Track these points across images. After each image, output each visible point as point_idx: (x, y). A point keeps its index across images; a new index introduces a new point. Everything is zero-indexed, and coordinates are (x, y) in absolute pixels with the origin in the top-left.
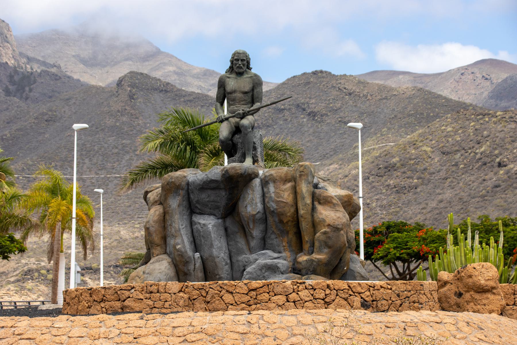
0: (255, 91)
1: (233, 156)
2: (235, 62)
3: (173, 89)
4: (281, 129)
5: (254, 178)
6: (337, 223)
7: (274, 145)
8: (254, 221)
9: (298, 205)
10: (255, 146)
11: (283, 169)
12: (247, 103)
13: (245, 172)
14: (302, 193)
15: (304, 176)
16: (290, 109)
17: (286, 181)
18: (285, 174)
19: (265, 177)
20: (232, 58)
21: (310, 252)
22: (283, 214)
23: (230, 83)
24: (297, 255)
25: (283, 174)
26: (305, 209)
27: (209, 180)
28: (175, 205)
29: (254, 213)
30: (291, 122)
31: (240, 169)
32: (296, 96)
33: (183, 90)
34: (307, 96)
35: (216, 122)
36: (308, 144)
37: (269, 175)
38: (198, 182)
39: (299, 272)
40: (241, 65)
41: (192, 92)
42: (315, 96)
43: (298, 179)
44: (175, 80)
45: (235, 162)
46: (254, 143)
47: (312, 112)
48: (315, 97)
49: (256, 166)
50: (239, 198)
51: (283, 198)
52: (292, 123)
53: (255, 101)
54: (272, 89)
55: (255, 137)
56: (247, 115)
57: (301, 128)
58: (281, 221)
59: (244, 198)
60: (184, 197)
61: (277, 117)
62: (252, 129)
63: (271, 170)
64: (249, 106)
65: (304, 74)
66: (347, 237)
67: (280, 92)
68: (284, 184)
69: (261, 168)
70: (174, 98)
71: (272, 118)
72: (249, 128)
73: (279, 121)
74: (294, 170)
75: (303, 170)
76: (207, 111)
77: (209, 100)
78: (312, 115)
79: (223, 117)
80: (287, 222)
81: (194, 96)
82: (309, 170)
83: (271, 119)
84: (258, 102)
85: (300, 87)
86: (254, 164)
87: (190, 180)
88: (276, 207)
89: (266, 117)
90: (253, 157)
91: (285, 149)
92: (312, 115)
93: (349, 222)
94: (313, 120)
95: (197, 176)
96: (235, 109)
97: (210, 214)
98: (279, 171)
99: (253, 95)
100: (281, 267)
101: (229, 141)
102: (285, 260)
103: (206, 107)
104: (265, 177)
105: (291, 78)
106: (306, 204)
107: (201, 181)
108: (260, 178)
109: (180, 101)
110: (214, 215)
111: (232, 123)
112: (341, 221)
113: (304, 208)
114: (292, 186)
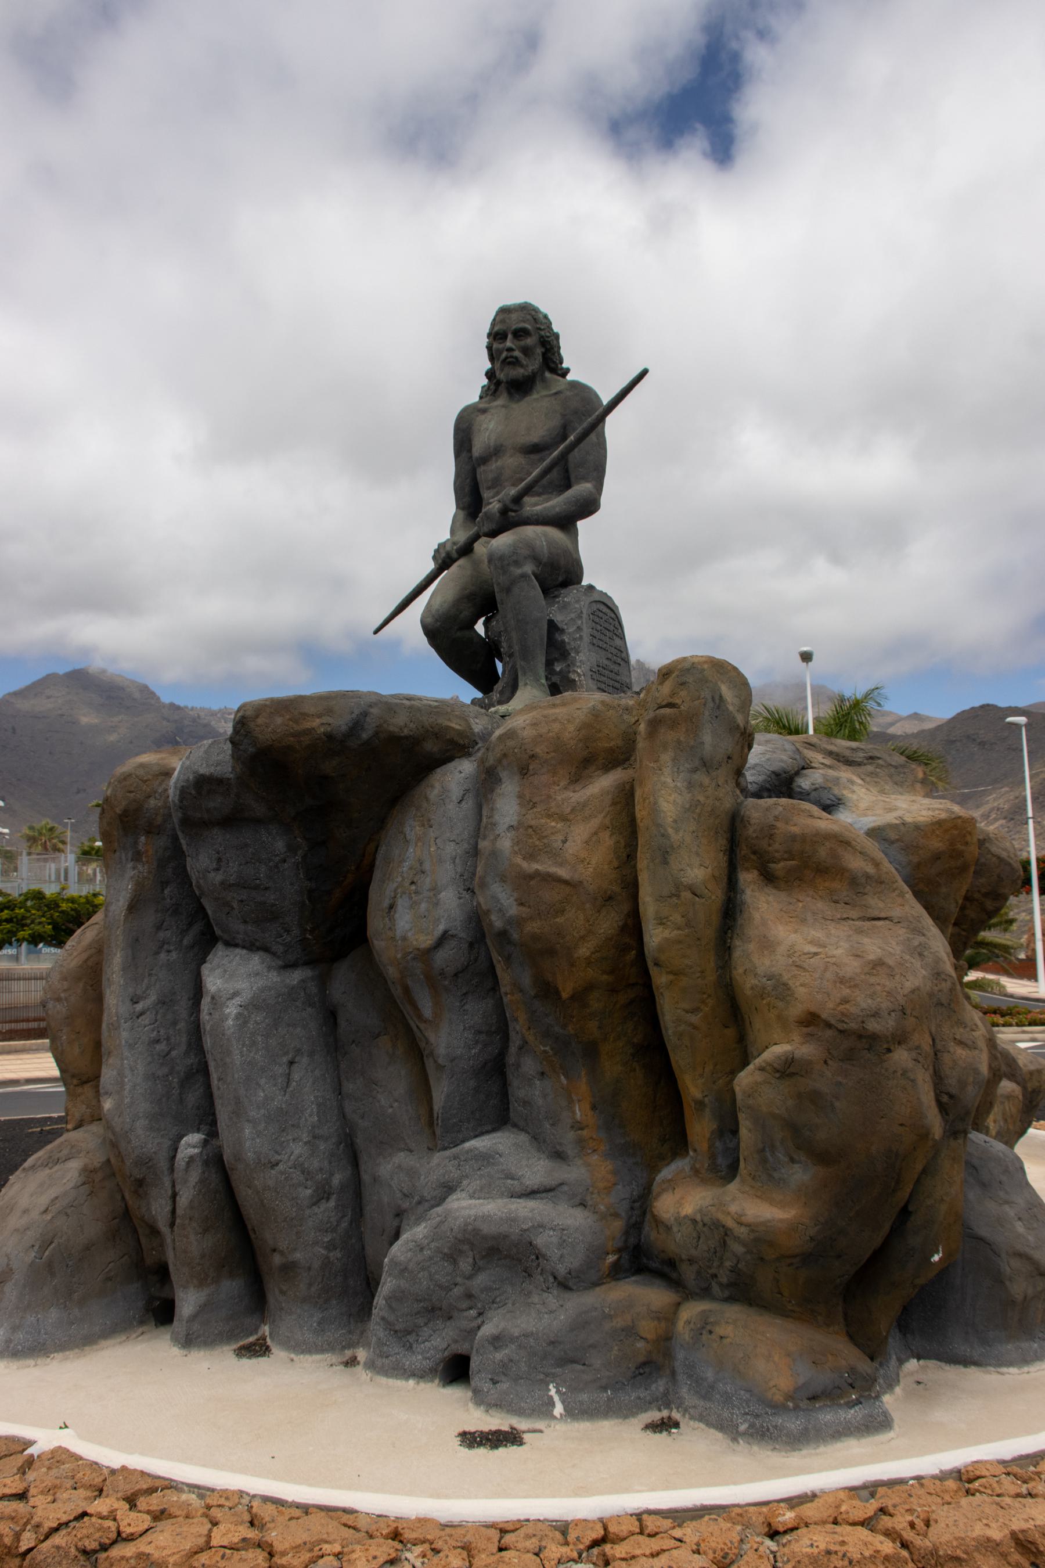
6: (863, 1001)
8: (432, 981)
15: (674, 724)
18: (585, 726)
21: (722, 1162)
22: (551, 952)
24: (653, 1169)
25: (571, 728)
26: (676, 918)
29: (425, 941)
31: (329, 711)
39: (666, 1269)
40: (517, 353)
47: (982, 742)
50: (372, 866)
51: (555, 855)
53: (573, 479)
58: (547, 991)
65: (973, 708)
66: (938, 1079)
75: (673, 694)
78: (982, 744)
80: (580, 997)
84: (584, 479)
88: (514, 910)
92: (982, 744)
93: (946, 986)
97: (252, 946)
98: (557, 711)
100: (554, 1253)
102: (583, 1204)
110: (266, 949)
112: (889, 984)
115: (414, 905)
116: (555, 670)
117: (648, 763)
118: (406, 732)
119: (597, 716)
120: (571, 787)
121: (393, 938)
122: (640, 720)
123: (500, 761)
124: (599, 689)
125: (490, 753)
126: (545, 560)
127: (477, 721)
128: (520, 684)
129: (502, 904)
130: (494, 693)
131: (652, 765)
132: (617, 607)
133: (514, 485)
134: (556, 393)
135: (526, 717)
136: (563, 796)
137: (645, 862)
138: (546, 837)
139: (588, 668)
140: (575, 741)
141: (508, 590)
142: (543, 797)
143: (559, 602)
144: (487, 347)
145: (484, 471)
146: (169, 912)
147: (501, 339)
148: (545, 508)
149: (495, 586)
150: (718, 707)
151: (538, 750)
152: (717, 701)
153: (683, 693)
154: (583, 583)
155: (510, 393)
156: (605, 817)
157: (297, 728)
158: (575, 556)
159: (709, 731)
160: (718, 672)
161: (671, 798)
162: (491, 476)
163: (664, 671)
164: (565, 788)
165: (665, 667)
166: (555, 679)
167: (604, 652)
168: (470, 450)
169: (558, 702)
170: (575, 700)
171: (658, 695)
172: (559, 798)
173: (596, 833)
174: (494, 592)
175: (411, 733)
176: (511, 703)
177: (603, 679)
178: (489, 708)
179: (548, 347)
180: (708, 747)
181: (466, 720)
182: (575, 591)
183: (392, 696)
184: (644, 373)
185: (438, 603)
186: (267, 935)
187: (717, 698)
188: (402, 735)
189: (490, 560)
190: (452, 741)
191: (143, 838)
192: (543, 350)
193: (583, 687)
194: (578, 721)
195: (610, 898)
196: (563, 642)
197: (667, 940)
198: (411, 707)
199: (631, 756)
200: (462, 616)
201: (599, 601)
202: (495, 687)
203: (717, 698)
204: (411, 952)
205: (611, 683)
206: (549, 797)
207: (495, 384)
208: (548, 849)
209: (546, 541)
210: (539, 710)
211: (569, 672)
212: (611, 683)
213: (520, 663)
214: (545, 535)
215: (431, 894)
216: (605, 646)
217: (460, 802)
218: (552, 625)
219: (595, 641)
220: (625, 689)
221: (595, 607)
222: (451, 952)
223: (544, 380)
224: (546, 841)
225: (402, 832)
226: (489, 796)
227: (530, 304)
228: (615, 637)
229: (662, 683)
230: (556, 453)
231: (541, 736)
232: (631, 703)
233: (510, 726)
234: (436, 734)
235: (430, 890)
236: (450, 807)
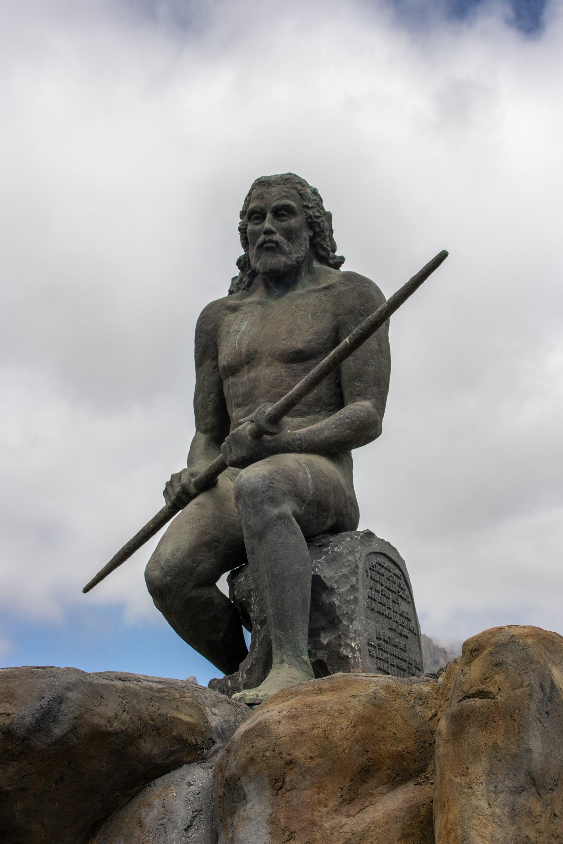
25: (344, 723)
40: (277, 237)
75: (485, 679)
84: (362, 395)
98: (324, 698)
116: (321, 643)
118: (116, 725)
119: (378, 707)
122: (439, 715)
123: (244, 769)
124: (379, 669)
125: (231, 758)
126: (310, 498)
127: (216, 711)
128: (274, 661)
130: (240, 672)
131: (458, 780)
132: (403, 561)
133: (272, 401)
134: (327, 288)
135: (281, 706)
136: (333, 822)
139: (365, 641)
140: (349, 742)
141: (261, 535)
142: (304, 824)
143: (328, 552)
144: (240, 229)
145: (232, 383)
147: (257, 218)
148: (310, 431)
149: (244, 530)
150: (550, 699)
151: (298, 753)
152: (548, 691)
153: (499, 678)
154: (358, 530)
155: (268, 288)
158: (348, 494)
159: (537, 733)
160: (547, 648)
162: (241, 390)
163: (472, 646)
165: (472, 640)
166: (322, 655)
167: (386, 620)
168: (215, 358)
169: (326, 686)
170: (349, 683)
172: (327, 825)
174: (242, 538)
175: (123, 728)
176: (261, 687)
177: (385, 656)
178: (233, 693)
179: (317, 230)
180: (537, 756)
181: (201, 710)
182: (348, 539)
183: (100, 675)
184: (442, 257)
185: (169, 551)
187: (547, 684)
188: (111, 729)
189: (238, 497)
190: (179, 739)
192: (311, 234)
193: (357, 666)
194: (353, 713)
196: (332, 605)
198: (124, 690)
199: (427, 765)
200: (200, 568)
201: (380, 553)
202: (242, 665)
203: (547, 684)
205: (396, 662)
206: (313, 823)
207: (249, 275)
209: (311, 473)
210: (301, 696)
211: (340, 646)
212: (396, 662)
213: (275, 632)
214: (310, 465)
216: (387, 612)
217: (187, 829)
218: (318, 583)
219: (374, 606)
220: (415, 670)
221: (374, 560)
223: (311, 271)
226: (229, 821)
227: (295, 176)
228: (400, 600)
229: (469, 662)
230: (326, 360)
231: (303, 734)
232: (426, 689)
233: (260, 719)
234: (158, 729)
236: (173, 836)
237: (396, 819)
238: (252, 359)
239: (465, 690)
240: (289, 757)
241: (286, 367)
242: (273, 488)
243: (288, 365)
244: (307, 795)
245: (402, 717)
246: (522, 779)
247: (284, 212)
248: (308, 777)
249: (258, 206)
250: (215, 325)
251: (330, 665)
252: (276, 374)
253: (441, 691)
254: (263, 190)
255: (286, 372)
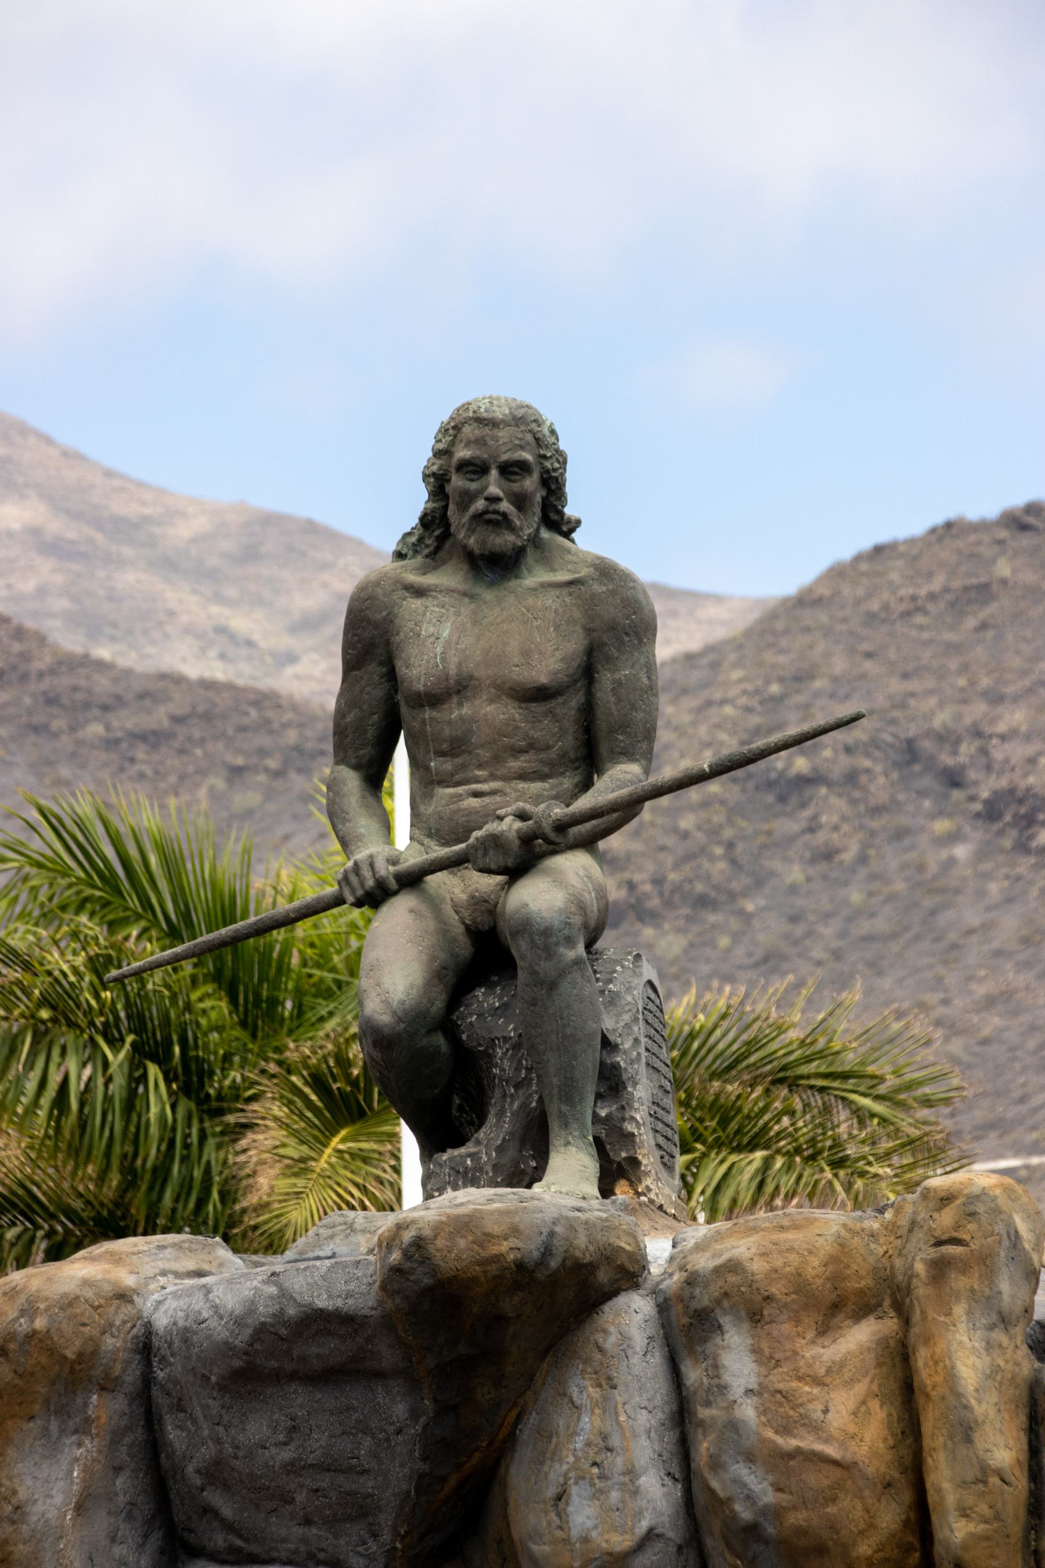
0: (606, 679)
1: (460, 1141)
2: (457, 482)
3: (26, 657)
4: (794, 919)
5: (614, 1293)
7: (752, 1046)
9: (931, 1480)
10: (616, 1067)
11: (810, 1221)
12: (552, 764)
13: (547, 1251)
14: (959, 1395)
15: (964, 1266)
16: (851, 778)
17: (836, 1307)
19: (692, 1280)
20: (438, 454)
23: (427, 629)
25: (815, 1261)
26: (984, 1509)
27: (292, 1311)
28: (58, 1499)
29: (621, 1542)
30: (863, 872)
31: (515, 1231)
32: (896, 686)
33: (101, 665)
34: (972, 683)
35: (338, 901)
36: (993, 1022)
37: (717, 1271)
38: (219, 1331)
40: (505, 506)
41: (163, 676)
42: (1027, 682)
43: (921, 1290)
44: (42, 592)
45: (474, 1182)
46: (607, 1044)
48: (1030, 691)
49: (626, 1208)
50: (511, 1439)
51: (816, 1428)
52: (873, 877)
53: (603, 749)
54: (726, 643)
55: (613, 1000)
56: (555, 850)
57: (933, 913)
59: (545, 1434)
60: (116, 1438)
61: (762, 839)
62: (589, 946)
63: (730, 1233)
64: (567, 782)
67: (782, 659)
68: (824, 1331)
69: (662, 1220)
70: (38, 719)
71: (730, 846)
72: (570, 942)
73: (777, 865)
74: (891, 1228)
75: (957, 1227)
76: (271, 807)
77: (285, 726)
79: (384, 870)
81: (179, 705)
82: (1000, 1228)
83: (719, 851)
84: (627, 754)
85: (919, 619)
86: (606, 1191)
87: (161, 1321)
88: (769, 1497)
89: (685, 835)
90: (599, 1144)
91: (827, 1076)
94: (1023, 847)
95: (207, 1290)
96: (471, 812)
98: (790, 1235)
99: (588, 711)
101: (430, 1032)
103: (262, 778)
104: (692, 1280)
105: (858, 558)
106: (984, 1472)
107: (239, 1322)
108: (654, 1292)
109: (80, 743)
111: (448, 909)
113: (970, 1500)
114: (883, 1343)
115: (598, 1494)
117: (935, 1315)
120: (819, 1341)
121: (566, 1541)
123: (718, 1302)
129: (750, 1490)
137: (941, 1439)
138: (802, 1405)
140: (821, 1280)
142: (788, 1354)
146: (123, 1515)
152: (1013, 1238)
153: (972, 1227)
156: (872, 1382)
157: (483, 1254)
159: (1006, 1277)
161: (970, 1362)
164: (813, 1342)
171: (934, 1226)
172: (808, 1355)
173: (864, 1402)
180: (1006, 1297)
186: (342, 1542)
187: (1012, 1232)
191: (95, 1397)
194: (823, 1252)
195: (889, 1485)
197: (972, 1535)
200: (434, 1009)
203: (1012, 1232)
204: (596, 1559)
206: (795, 1353)
208: (806, 1421)
211: (624, 1119)
215: (627, 1479)
222: (654, 1558)
224: (801, 1410)
225: (565, 1394)
231: (776, 1271)
235: (624, 1474)
237: (869, 1349)
238: (465, 687)
239: (936, 1235)
240: (766, 1293)
241: (520, 708)
242: (570, 924)
243: (523, 705)
244: (786, 1328)
245: (862, 1255)
246: (994, 1317)
247: (516, 470)
248: (785, 1312)
249: (478, 458)
250: (389, 614)
251: (610, 1144)
252: (507, 717)
253: (890, 1227)
254: (484, 433)
255: (520, 714)
